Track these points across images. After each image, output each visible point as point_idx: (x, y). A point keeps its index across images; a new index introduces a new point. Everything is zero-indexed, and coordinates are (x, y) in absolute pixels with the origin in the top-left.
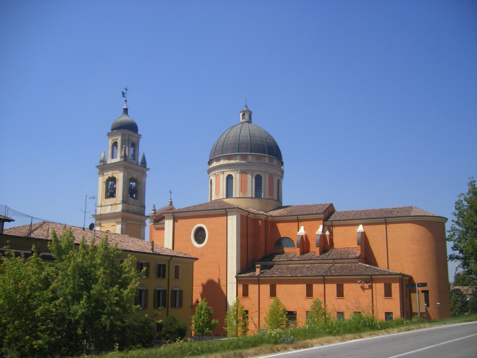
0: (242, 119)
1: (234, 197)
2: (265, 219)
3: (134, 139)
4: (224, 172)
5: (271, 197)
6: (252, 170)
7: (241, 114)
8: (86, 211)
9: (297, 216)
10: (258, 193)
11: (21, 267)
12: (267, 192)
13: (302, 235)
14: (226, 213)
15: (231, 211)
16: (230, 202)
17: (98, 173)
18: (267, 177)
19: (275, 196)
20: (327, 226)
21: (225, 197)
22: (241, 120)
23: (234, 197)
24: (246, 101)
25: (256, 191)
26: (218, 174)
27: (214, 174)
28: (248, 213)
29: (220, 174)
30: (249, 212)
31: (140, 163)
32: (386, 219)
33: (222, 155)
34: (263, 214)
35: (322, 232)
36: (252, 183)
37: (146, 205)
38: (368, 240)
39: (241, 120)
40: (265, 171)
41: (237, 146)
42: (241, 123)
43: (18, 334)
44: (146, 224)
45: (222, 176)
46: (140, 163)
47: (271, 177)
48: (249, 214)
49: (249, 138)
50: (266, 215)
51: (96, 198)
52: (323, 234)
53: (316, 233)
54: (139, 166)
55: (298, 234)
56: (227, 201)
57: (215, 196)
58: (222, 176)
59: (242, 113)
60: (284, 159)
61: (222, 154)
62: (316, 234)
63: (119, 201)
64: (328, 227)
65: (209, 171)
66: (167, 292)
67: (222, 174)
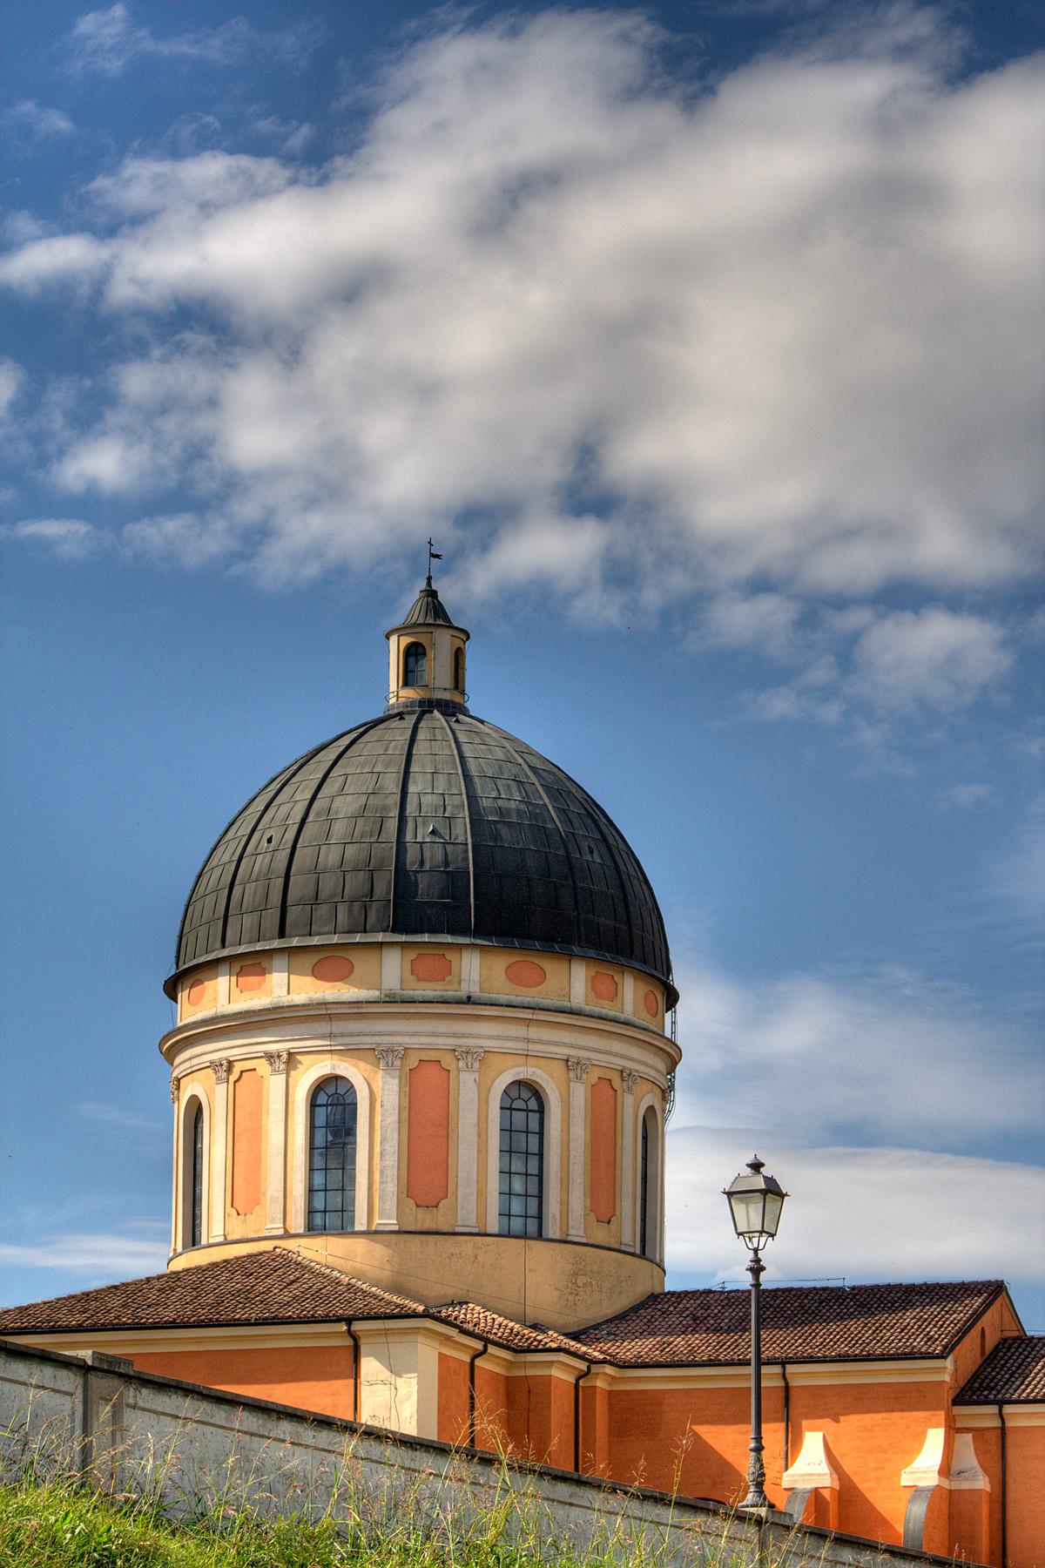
0: (406, 683)
2: (578, 1380)
4: (290, 1054)
5: (601, 1235)
6: (406, 1049)
7: (395, 648)
9: (349, 1321)
12: (578, 1201)
13: (810, 1486)
14: (349, 1342)
16: (309, 1254)
18: (579, 1094)
19: (628, 1233)
20: (969, 1437)
21: (298, 1222)
22: (393, 686)
23: (360, 1224)
27: (214, 1066)
28: (479, 1345)
29: (263, 1067)
30: (487, 1341)
32: (790, 1369)
33: (276, 944)
34: (567, 1352)
35: (940, 1472)
36: (310, 1047)
39: (395, 692)
41: (384, 885)
42: (401, 716)
48: (485, 1347)
49: (462, 831)
50: (582, 1357)
52: (946, 1484)
53: (906, 1479)
55: (785, 1485)
56: (320, 1251)
58: (276, 1083)
59: (405, 641)
61: (282, 934)
62: (904, 1482)
65: (176, 1043)
67: (275, 1072)
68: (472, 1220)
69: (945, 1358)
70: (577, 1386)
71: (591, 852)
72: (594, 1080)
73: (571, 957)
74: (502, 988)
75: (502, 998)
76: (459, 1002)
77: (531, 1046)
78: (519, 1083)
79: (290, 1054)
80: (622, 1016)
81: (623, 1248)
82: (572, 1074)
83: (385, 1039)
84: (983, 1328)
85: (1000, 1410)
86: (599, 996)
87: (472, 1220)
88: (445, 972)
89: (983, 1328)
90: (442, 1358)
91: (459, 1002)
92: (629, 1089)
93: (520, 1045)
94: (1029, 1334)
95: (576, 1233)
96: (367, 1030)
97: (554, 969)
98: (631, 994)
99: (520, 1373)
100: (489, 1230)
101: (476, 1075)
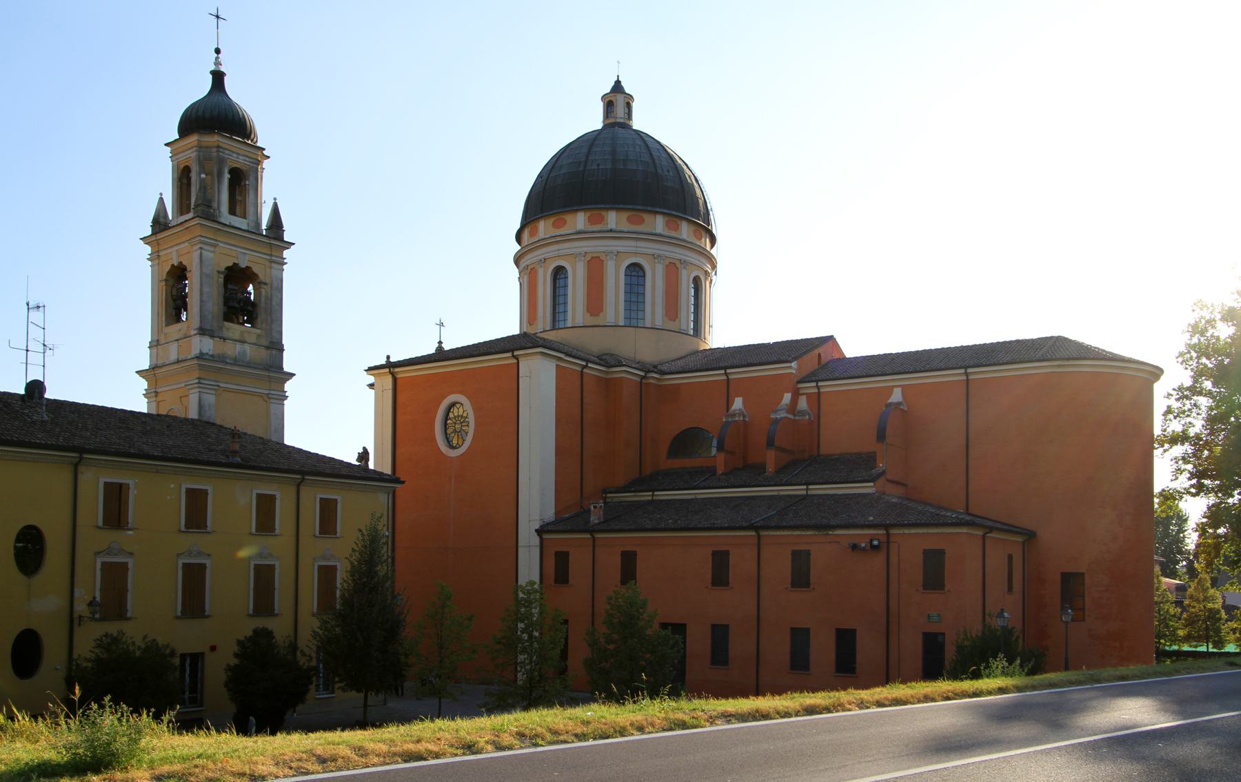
1: (569, 324)
3: (240, 161)
4: (545, 259)
6: (586, 253)
8: (29, 349)
10: (633, 315)
11: (521, 673)
12: (660, 310)
15: (526, 354)
17: (149, 257)
18: (660, 269)
20: (805, 397)
24: (218, 51)
25: (628, 309)
26: (532, 267)
30: (588, 361)
31: (264, 226)
37: (286, 341)
38: (416, 357)
40: (681, 260)
43: (147, 758)
44: (287, 394)
45: (540, 272)
46: (264, 226)
47: (672, 271)
48: (587, 364)
51: (44, 306)
54: (263, 235)
57: (527, 326)
60: (718, 228)
63: (195, 330)
64: (807, 398)
66: (854, 675)
68: (613, 321)
69: (791, 362)
70: (641, 382)
71: (668, 172)
72: (667, 263)
73: (577, 211)
74: (625, 226)
75: (626, 230)
76: (607, 231)
77: (638, 249)
78: (628, 267)
79: (545, 259)
80: (681, 238)
81: (682, 331)
82: (656, 260)
83: (683, 257)
84: (819, 354)
85: (817, 384)
86: (669, 229)
87: (613, 321)
88: (601, 220)
89: (819, 354)
90: (557, 366)
91: (607, 231)
92: (685, 268)
93: (635, 249)
94: (847, 356)
95: (659, 323)
96: (661, 248)
97: (569, 218)
98: (685, 231)
99: (610, 376)
100: (620, 324)
101: (614, 262)
